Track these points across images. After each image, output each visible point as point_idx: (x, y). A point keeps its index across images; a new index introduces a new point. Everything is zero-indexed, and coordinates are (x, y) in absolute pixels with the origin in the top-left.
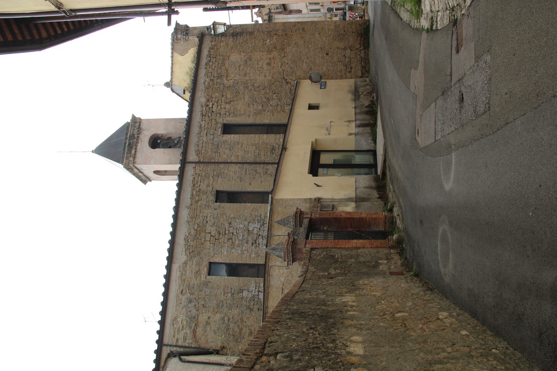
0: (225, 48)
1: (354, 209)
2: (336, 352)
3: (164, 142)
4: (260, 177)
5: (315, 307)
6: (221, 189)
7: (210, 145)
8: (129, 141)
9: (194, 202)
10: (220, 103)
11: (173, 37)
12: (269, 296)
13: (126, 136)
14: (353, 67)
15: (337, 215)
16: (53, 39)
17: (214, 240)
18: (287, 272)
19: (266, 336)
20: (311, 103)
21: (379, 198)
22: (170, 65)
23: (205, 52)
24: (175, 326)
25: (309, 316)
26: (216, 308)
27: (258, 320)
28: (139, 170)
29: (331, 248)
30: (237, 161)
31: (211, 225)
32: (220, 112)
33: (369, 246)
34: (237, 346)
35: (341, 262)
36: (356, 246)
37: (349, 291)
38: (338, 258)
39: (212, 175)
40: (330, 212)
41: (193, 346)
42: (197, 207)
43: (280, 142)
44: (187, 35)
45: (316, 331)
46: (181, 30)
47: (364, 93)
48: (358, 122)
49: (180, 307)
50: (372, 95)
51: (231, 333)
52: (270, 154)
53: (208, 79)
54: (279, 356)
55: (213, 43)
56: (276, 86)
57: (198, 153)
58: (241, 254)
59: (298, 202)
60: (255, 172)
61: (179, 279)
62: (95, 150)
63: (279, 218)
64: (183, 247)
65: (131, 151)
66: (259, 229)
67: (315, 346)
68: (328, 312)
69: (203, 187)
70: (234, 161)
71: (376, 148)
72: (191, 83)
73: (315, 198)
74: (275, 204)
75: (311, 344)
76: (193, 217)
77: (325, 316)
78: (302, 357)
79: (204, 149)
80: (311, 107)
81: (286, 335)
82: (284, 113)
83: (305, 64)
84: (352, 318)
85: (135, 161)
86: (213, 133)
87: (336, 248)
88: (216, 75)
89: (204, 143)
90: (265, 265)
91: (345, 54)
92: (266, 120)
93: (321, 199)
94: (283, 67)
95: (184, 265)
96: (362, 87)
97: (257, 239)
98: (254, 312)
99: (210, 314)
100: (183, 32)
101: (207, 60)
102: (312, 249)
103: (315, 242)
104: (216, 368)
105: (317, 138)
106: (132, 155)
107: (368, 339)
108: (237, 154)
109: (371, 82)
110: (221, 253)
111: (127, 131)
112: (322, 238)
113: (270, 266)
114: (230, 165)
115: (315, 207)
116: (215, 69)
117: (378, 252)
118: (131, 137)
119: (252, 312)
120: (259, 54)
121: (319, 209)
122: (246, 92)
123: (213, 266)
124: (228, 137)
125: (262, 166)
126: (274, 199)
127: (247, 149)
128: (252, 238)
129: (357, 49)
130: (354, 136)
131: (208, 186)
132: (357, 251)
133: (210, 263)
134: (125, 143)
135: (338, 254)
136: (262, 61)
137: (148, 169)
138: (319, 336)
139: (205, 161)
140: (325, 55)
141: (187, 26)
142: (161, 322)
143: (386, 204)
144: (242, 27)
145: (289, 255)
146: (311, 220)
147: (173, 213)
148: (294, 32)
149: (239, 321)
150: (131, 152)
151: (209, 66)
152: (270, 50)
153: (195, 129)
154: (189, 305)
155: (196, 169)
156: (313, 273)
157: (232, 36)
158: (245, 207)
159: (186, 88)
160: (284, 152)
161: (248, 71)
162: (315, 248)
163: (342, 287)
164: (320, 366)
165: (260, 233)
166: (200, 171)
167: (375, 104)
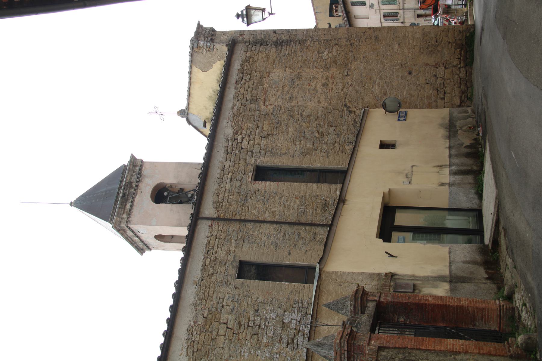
0: (264, 61)
1: (448, 292)
3: (172, 195)
4: (305, 244)
6: (247, 258)
8: (123, 191)
10: (253, 137)
11: (193, 44)
13: (120, 184)
14: (448, 92)
15: (421, 300)
17: (232, 334)
20: (381, 139)
21: (487, 279)
22: (187, 85)
23: (236, 66)
31: (228, 311)
36: (453, 348)
39: (236, 238)
42: (210, 283)
44: (212, 42)
47: (464, 128)
48: (454, 168)
52: (321, 211)
53: (237, 103)
55: (248, 54)
56: (333, 117)
57: (217, 205)
58: (270, 359)
59: (361, 278)
60: (297, 237)
63: (330, 300)
64: (184, 344)
65: (126, 205)
66: (299, 322)
69: (221, 255)
70: (268, 219)
71: (481, 206)
74: (324, 279)
79: (226, 201)
80: (383, 145)
83: (377, 86)
87: (420, 349)
88: (249, 98)
89: (227, 191)
94: (345, 90)
103: (384, 338)
105: (391, 187)
106: (126, 211)
108: (273, 210)
109: (475, 113)
111: (123, 177)
114: (262, 224)
115: (385, 286)
116: (249, 90)
118: (128, 185)
120: (311, 70)
121: (391, 289)
122: (291, 123)
124: (261, 185)
125: (308, 228)
127: (288, 203)
128: (288, 335)
129: (455, 66)
130: (447, 187)
131: (228, 253)
134: (118, 194)
136: (315, 81)
140: (406, 74)
141: (213, 30)
143: (500, 288)
144: (290, 34)
145: (343, 356)
146: (379, 305)
148: (364, 41)
150: (125, 207)
151: (240, 85)
153: (215, 172)
155: (212, 229)
158: (281, 287)
159: (208, 119)
160: (341, 205)
161: (295, 94)
165: (301, 328)
166: (218, 231)
167: (480, 144)
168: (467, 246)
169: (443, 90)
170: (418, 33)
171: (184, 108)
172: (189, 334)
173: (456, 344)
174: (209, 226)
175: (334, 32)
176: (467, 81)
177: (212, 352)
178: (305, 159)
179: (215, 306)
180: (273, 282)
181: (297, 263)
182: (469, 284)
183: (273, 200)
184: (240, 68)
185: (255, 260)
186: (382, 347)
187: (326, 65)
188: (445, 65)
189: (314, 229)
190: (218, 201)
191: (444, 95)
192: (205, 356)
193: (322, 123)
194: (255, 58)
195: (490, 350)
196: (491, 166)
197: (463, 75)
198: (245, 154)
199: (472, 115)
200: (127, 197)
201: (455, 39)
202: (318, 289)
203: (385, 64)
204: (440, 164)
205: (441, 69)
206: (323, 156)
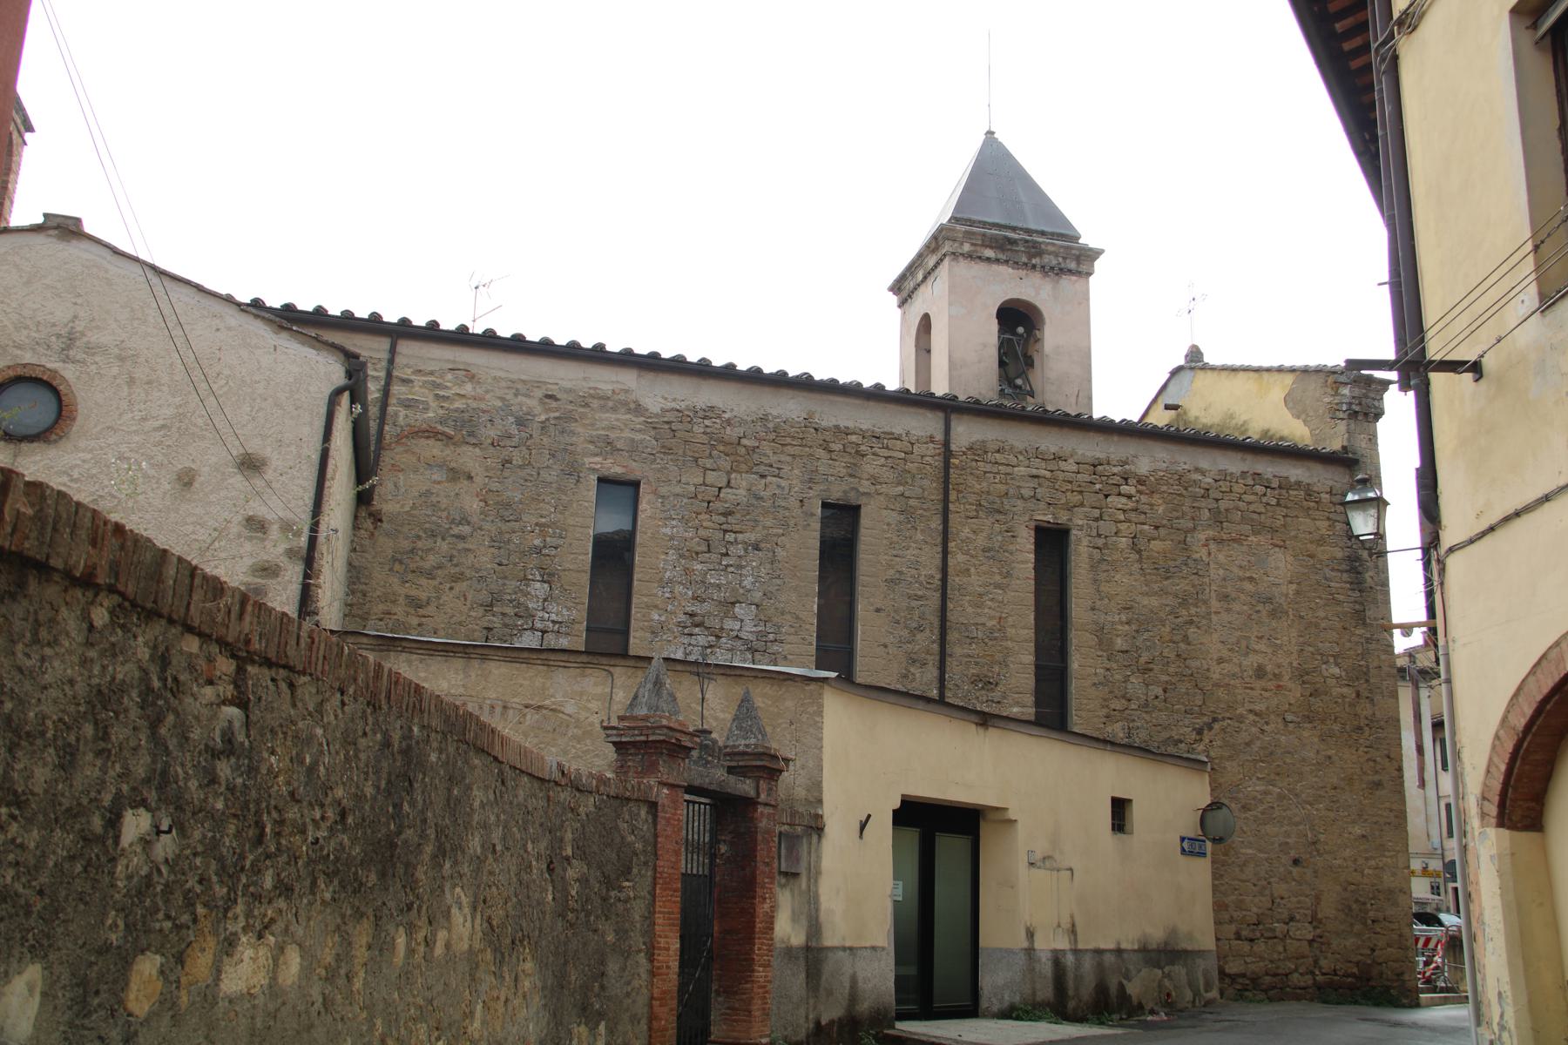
0: (1310, 533)
1: (783, 942)
2: (235, 901)
4: (900, 641)
5: (431, 822)
6: (865, 521)
7: (1003, 488)
8: (1021, 240)
9: (825, 437)
12: (518, 665)
13: (1036, 232)
14: (1255, 948)
16: (1316, 9)
17: (706, 498)
18: (592, 724)
19: (319, 668)
21: (818, 1023)
22: (1255, 363)
23: (1295, 472)
24: (449, 376)
25: (395, 806)
26: (500, 499)
27: (458, 627)
28: (933, 270)
29: (655, 866)
30: (950, 570)
31: (754, 488)
32: (1106, 518)
33: (656, 991)
34: (381, 560)
35: (605, 899)
36: (660, 949)
37: (494, 931)
38: (621, 889)
39: (907, 494)
40: (776, 865)
41: (387, 428)
42: (810, 447)
43: (1011, 706)
44: (1350, 414)
45: (331, 829)
46: (1366, 396)
47: (1167, 982)
49: (507, 391)
50: (1163, 1006)
51: (420, 544)
52: (973, 675)
53: (1210, 480)
54: (232, 712)
56: (1188, 694)
59: (811, 764)
60: (914, 625)
61: (590, 388)
62: (1001, 146)
63: (759, 702)
64: (686, 403)
65: (991, 248)
66: (737, 636)
67: (268, 830)
68: (407, 865)
69: (871, 466)
70: (951, 562)
71: (985, 1016)
72: (1198, 427)
73: (822, 817)
75: (275, 815)
76: (779, 434)
77: (392, 856)
78: (223, 789)
79: (988, 467)
80: (1120, 807)
81: (319, 731)
82: (1104, 720)
83: (1263, 788)
84: (382, 946)
85: (961, 259)
86: (1039, 496)
87: (655, 884)
88: (1223, 505)
89: (1009, 470)
90: (624, 655)
91: (1298, 921)
92: (1083, 663)
93: (820, 837)
94: (1252, 717)
95: (632, 406)
96: (1187, 974)
97: (707, 628)
98: (480, 615)
99: (479, 480)
100: (1360, 404)
101: (1270, 476)
102: (653, 806)
103: (675, 814)
104: (306, 498)
105: (1020, 826)
106: (978, 248)
107: (284, 1004)
108: (973, 570)
109: (1205, 1006)
110: (665, 519)
112: (690, 837)
113: (611, 669)
114: (939, 549)
117: (634, 1019)
118: (1033, 247)
119: (481, 610)
122: (1169, 600)
123: (630, 491)
124: (1025, 544)
125: (936, 647)
126: (822, 687)
127: (989, 603)
128: (710, 614)
129: (1316, 962)
130: (1025, 944)
131: (875, 480)
132: (640, 951)
133: (636, 485)
135: (635, 888)
136: (1269, 651)
137: (934, 297)
138: (310, 839)
139: (951, 471)
140: (1293, 853)
141: (1379, 414)
142: (462, 333)
144: (1379, 588)
145: (636, 732)
146: (749, 803)
147: (791, 374)
148: (1369, 756)
149: (457, 569)
150: (986, 246)
151: (1252, 483)
152: (1305, 678)
153: (1051, 441)
154: (511, 419)
156: (572, 810)
157: (1348, 557)
158: (807, 595)
159: (1185, 413)
161: (1236, 607)
162: (655, 817)
163: (509, 904)
164: (182, 850)
165: (724, 640)
166: (922, 456)
167: (1130, 1016)
168: (891, 984)
169: (1258, 935)
170: (1392, 879)
171: (1206, 360)
172: (704, 411)
173: (668, 955)
174: (931, 437)
175: (1387, 688)
176: (1281, 989)
177: (671, 460)
178: (1088, 634)
179: (764, 459)
180: (817, 578)
181: (859, 627)
182: (804, 985)
183: (995, 570)
184: (1292, 480)
185: (862, 538)
186: (656, 811)
187: (1307, 674)
188: (1319, 940)
189: (933, 660)
190: (986, 452)
191: (1246, 939)
192: (663, 447)
193: (1171, 670)
194: (1317, 512)
195: (661, 1019)
196: (1066, 1037)
197: (1296, 981)
198: (1094, 504)
199: (1200, 1002)
200: (1008, 250)
201: (1381, 964)
202: (786, 677)
203: (1316, 806)
204: (1079, 930)
205: (1307, 932)
206: (1096, 674)
